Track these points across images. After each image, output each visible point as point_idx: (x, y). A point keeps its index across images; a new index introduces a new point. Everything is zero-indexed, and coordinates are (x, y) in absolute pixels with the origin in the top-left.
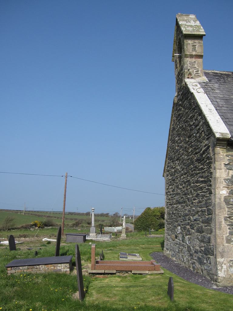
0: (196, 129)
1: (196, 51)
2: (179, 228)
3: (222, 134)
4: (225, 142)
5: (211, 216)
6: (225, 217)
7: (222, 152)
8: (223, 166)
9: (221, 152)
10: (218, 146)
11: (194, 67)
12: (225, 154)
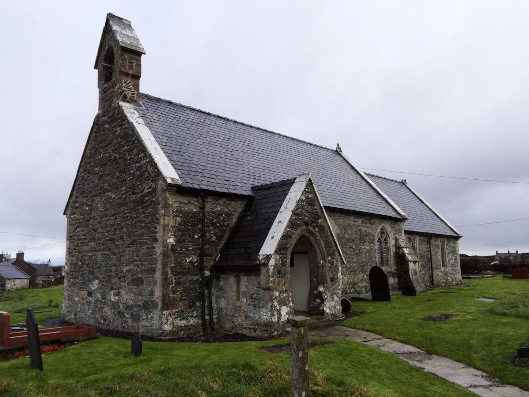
0: (395, 335)
1: (133, 70)
2: (97, 281)
3: (173, 179)
4: (175, 189)
5: (155, 266)
6: (172, 267)
7: (171, 199)
8: (171, 212)
9: (170, 198)
10: (168, 191)
11: (130, 89)
12: (173, 201)
